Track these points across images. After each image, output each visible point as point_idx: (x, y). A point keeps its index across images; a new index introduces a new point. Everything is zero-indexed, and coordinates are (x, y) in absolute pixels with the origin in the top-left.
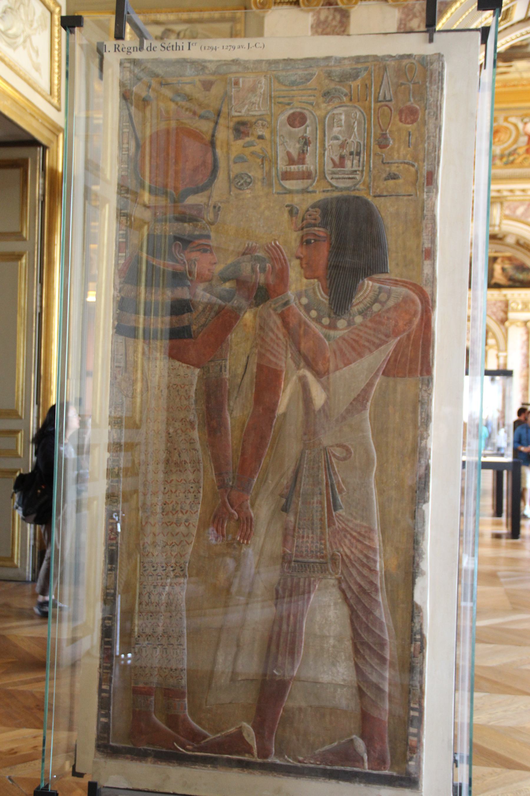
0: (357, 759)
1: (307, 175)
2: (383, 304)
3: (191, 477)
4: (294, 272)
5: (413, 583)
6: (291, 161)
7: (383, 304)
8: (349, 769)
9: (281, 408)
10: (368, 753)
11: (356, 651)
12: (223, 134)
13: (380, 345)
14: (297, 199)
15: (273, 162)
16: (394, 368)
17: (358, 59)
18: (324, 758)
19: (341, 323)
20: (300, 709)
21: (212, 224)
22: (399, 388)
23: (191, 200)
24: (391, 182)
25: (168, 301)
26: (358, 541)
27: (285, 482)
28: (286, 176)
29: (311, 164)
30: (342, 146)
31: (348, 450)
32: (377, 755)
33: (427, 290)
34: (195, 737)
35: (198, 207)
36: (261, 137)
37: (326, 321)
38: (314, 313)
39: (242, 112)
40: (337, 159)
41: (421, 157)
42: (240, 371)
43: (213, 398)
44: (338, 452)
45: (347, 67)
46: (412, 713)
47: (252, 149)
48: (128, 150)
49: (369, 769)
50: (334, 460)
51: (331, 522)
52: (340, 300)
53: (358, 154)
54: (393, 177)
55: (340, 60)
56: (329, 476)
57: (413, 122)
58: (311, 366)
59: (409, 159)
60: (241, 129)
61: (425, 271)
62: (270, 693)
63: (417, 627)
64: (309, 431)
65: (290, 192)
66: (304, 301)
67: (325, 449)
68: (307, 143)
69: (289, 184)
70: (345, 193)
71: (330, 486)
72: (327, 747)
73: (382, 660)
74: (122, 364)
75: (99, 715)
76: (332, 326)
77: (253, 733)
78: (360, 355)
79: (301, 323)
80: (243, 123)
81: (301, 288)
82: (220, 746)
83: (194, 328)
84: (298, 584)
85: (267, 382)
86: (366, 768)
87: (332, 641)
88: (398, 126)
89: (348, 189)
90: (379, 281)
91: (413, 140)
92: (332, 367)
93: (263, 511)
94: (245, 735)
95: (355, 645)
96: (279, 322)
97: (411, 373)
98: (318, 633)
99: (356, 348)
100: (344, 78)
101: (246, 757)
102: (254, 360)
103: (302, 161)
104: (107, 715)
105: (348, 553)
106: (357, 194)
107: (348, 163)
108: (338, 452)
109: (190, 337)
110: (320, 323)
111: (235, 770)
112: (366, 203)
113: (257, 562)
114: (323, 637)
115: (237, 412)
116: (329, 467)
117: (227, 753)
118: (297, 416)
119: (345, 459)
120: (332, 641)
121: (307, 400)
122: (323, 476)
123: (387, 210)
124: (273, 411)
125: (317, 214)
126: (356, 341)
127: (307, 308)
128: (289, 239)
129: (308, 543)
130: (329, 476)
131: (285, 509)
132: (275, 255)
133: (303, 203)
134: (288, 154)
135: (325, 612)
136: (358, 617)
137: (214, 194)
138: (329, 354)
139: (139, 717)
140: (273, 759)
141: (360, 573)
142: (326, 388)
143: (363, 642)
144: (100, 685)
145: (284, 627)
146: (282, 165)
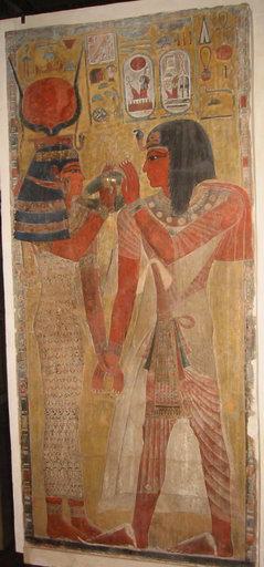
0: (209, 550)
1: (148, 106)
2: (213, 203)
3: (76, 345)
4: (143, 178)
5: (247, 421)
6: (136, 95)
7: (213, 203)
8: (203, 556)
9: (140, 289)
10: (217, 545)
11: (205, 472)
12: (83, 83)
13: (212, 237)
14: (142, 125)
15: (122, 99)
16: (222, 254)
17: (181, 13)
18: (185, 549)
19: (181, 221)
20: (166, 514)
21: (79, 149)
22: (228, 270)
23: (63, 132)
24: (214, 107)
25: (176, 112)
26: (202, 390)
27: (145, 346)
28: (133, 108)
29: (151, 96)
30: (175, 80)
31: (192, 320)
32: (224, 546)
33: (247, 190)
34: (91, 532)
35: (69, 139)
36: (112, 80)
37: (169, 220)
38: (160, 214)
39: (93, 63)
40: (171, 91)
41: (236, 85)
42: (107, 262)
43: (89, 285)
44: (184, 321)
45: (174, 19)
46: (249, 517)
47: (106, 89)
48: (15, 99)
49: (219, 555)
50: (181, 328)
51: (181, 374)
52: (180, 204)
53: (187, 86)
54: (216, 102)
55: (169, 15)
56: (178, 340)
57: (227, 58)
58: (159, 255)
59: (226, 87)
60: (96, 75)
61: (245, 176)
62: (145, 503)
63: (250, 452)
64: (162, 304)
65: (137, 120)
66: (152, 205)
67: (174, 320)
68: (147, 81)
69: (135, 114)
70: (178, 118)
71: (180, 350)
72: (187, 541)
73: (227, 479)
74: (21, 262)
75: (25, 517)
76: (175, 224)
77: (132, 531)
78: (197, 245)
79: (152, 222)
80: (98, 70)
81: (150, 194)
82: (110, 539)
83: (70, 231)
84: (159, 424)
85: (128, 269)
86: (215, 555)
87: (187, 465)
88: (215, 61)
89: (180, 114)
90: (206, 185)
91: (228, 73)
92: (176, 256)
93: (131, 367)
94: (127, 532)
95: (204, 468)
96: (134, 222)
97: (239, 257)
98: (176, 459)
99: (193, 240)
100: (173, 27)
101: (130, 547)
102: (117, 252)
103: (143, 94)
104: (31, 517)
105: (196, 399)
106: (187, 117)
107: (179, 93)
108: (184, 321)
109: (68, 237)
110: (165, 221)
111: (122, 556)
112: (196, 124)
113: (134, 396)
114: (180, 462)
115: (109, 292)
116: (177, 330)
117: (113, 544)
118: (153, 296)
119: (189, 327)
120: (187, 465)
121: (159, 283)
122: (173, 341)
123: (212, 129)
124: (134, 292)
125: (158, 135)
126: (194, 235)
127: (155, 210)
128: (139, 160)
129: (165, 393)
130: (178, 340)
131: (147, 367)
132: (129, 168)
133: (147, 129)
134: (133, 90)
135: (183, 445)
136: (206, 447)
137: (79, 126)
138: (174, 247)
139: (54, 520)
140: (149, 549)
141: (205, 414)
142: (172, 272)
143: (213, 463)
144: (23, 496)
145: (151, 455)
146: (129, 99)
